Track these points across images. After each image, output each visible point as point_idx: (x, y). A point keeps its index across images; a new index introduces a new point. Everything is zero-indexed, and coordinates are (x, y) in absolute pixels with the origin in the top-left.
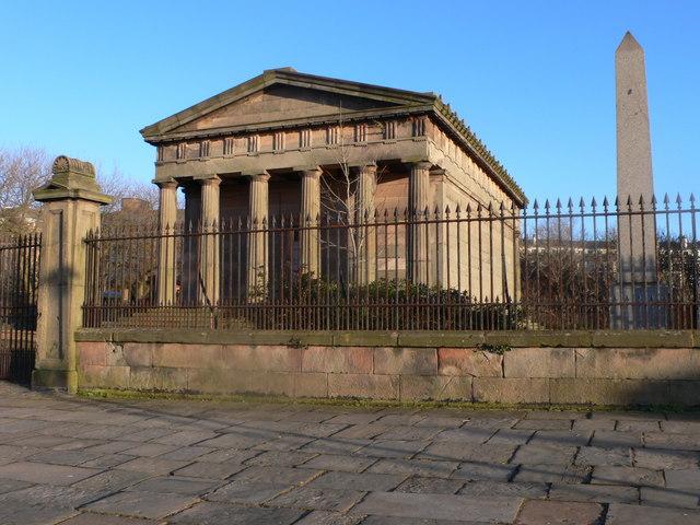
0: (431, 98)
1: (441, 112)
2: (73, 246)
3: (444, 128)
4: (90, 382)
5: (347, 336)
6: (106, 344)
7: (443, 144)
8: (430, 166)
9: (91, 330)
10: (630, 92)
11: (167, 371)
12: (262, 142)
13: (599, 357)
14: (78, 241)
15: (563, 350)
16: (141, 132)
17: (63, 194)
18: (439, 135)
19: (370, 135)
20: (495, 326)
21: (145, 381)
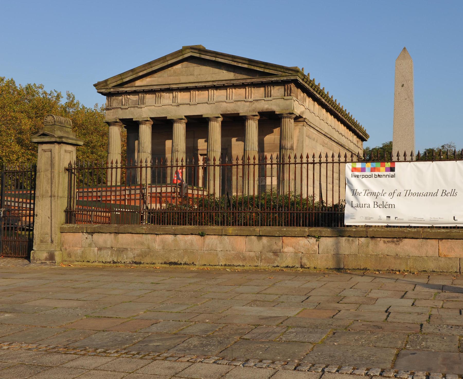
0: (296, 71)
1: (303, 80)
2: (59, 172)
3: (305, 90)
4: (71, 257)
5: (231, 229)
6: (81, 234)
7: (304, 100)
8: (294, 116)
9: (71, 225)
10: (403, 86)
11: (121, 251)
12: (182, 97)
13: (372, 243)
14: (62, 169)
15: (351, 239)
16: (95, 85)
17: (53, 140)
18: (302, 95)
19: (258, 93)
20: (157, 223)
21: (107, 256)
